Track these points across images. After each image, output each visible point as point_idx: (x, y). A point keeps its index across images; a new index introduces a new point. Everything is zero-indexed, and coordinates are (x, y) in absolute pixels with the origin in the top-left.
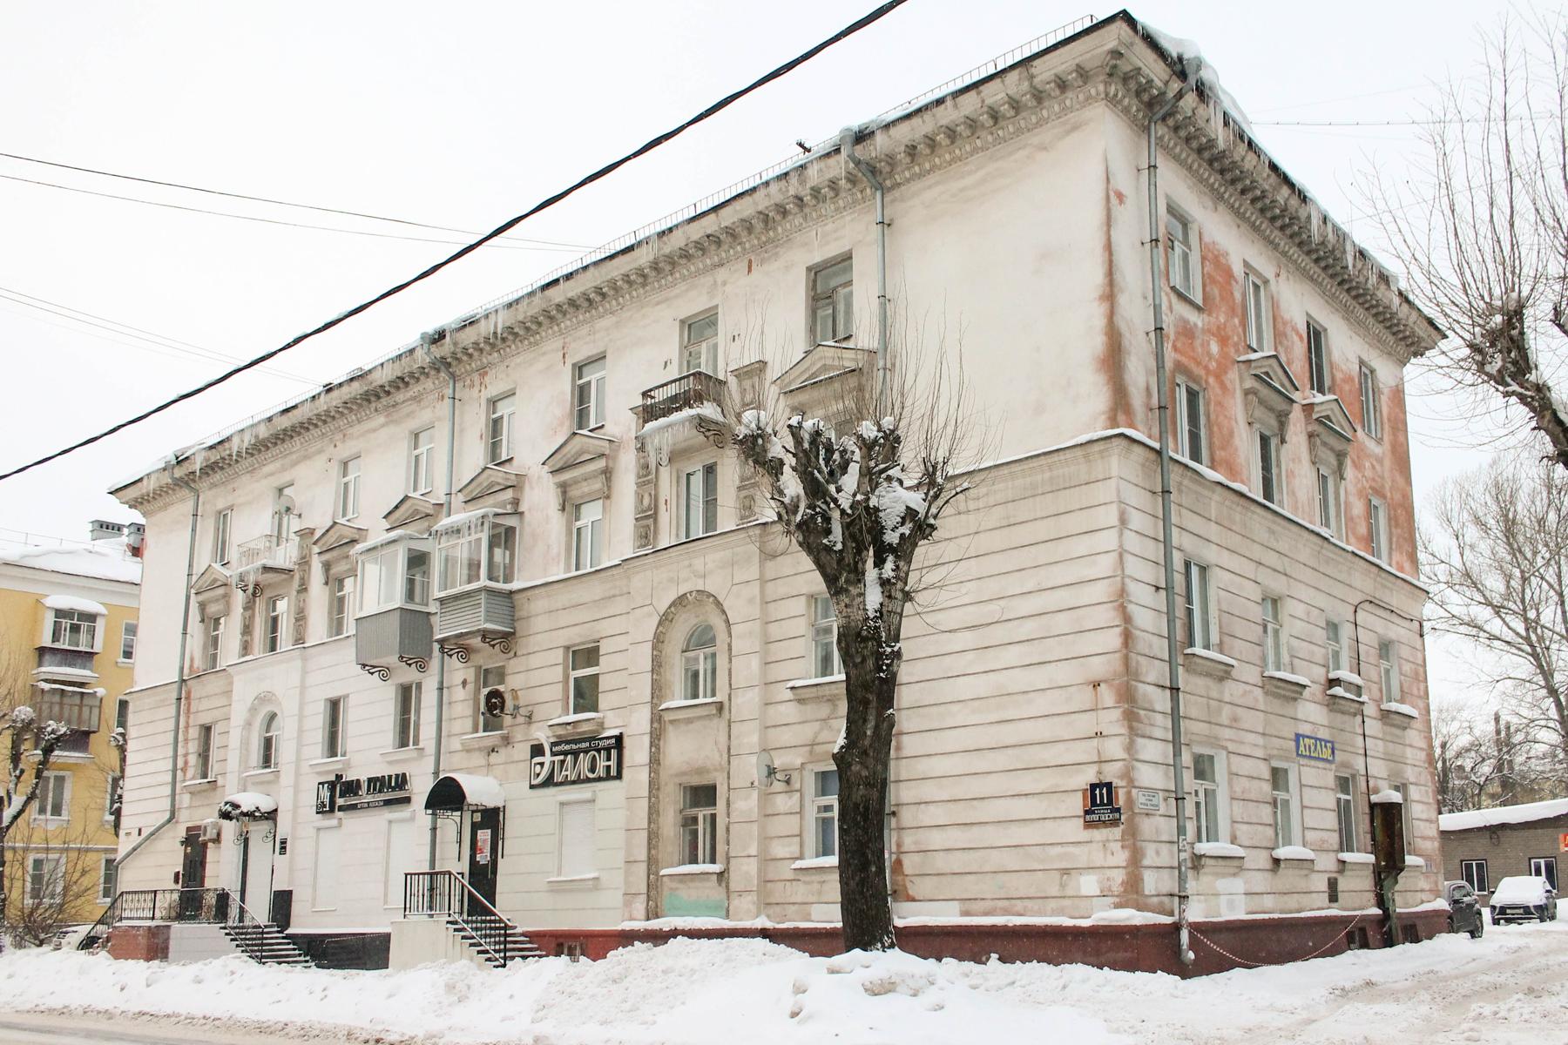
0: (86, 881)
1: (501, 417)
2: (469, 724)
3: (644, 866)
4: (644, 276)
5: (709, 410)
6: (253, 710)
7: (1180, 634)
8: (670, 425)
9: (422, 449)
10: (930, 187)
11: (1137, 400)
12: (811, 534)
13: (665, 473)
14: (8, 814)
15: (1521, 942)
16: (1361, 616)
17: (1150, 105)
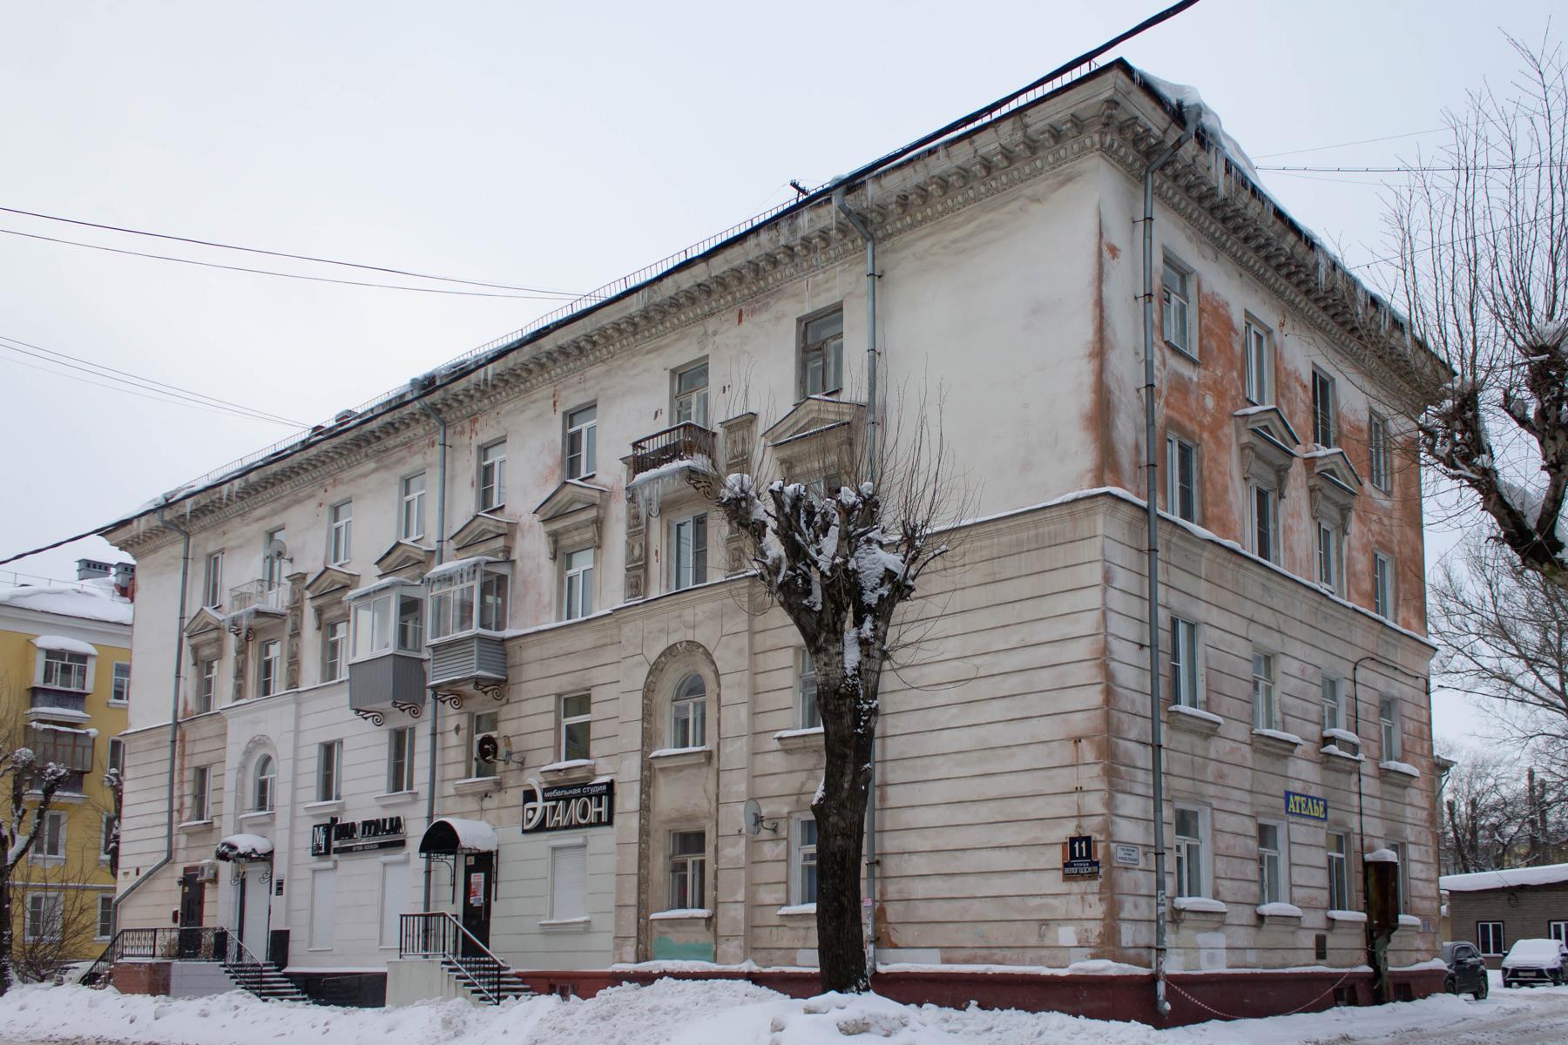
0: (84, 919)
1: (493, 465)
2: (462, 769)
3: (634, 911)
4: (635, 325)
5: (699, 462)
6: (248, 753)
7: (1163, 692)
8: (658, 477)
9: (414, 495)
10: (922, 238)
11: (1125, 459)
12: (792, 595)
13: (656, 524)
14: (12, 852)
15: (1522, 1004)
16: (1362, 674)
17: (1148, 154)
